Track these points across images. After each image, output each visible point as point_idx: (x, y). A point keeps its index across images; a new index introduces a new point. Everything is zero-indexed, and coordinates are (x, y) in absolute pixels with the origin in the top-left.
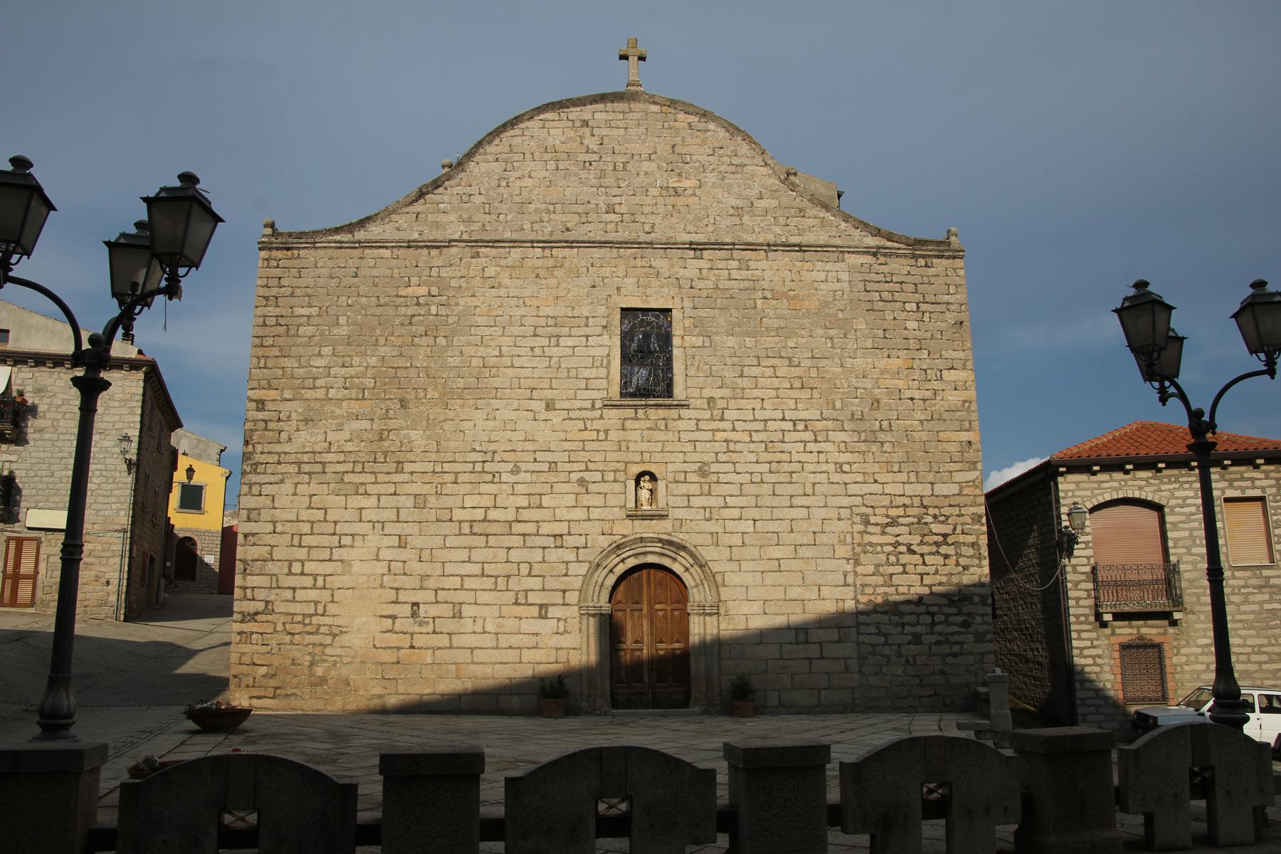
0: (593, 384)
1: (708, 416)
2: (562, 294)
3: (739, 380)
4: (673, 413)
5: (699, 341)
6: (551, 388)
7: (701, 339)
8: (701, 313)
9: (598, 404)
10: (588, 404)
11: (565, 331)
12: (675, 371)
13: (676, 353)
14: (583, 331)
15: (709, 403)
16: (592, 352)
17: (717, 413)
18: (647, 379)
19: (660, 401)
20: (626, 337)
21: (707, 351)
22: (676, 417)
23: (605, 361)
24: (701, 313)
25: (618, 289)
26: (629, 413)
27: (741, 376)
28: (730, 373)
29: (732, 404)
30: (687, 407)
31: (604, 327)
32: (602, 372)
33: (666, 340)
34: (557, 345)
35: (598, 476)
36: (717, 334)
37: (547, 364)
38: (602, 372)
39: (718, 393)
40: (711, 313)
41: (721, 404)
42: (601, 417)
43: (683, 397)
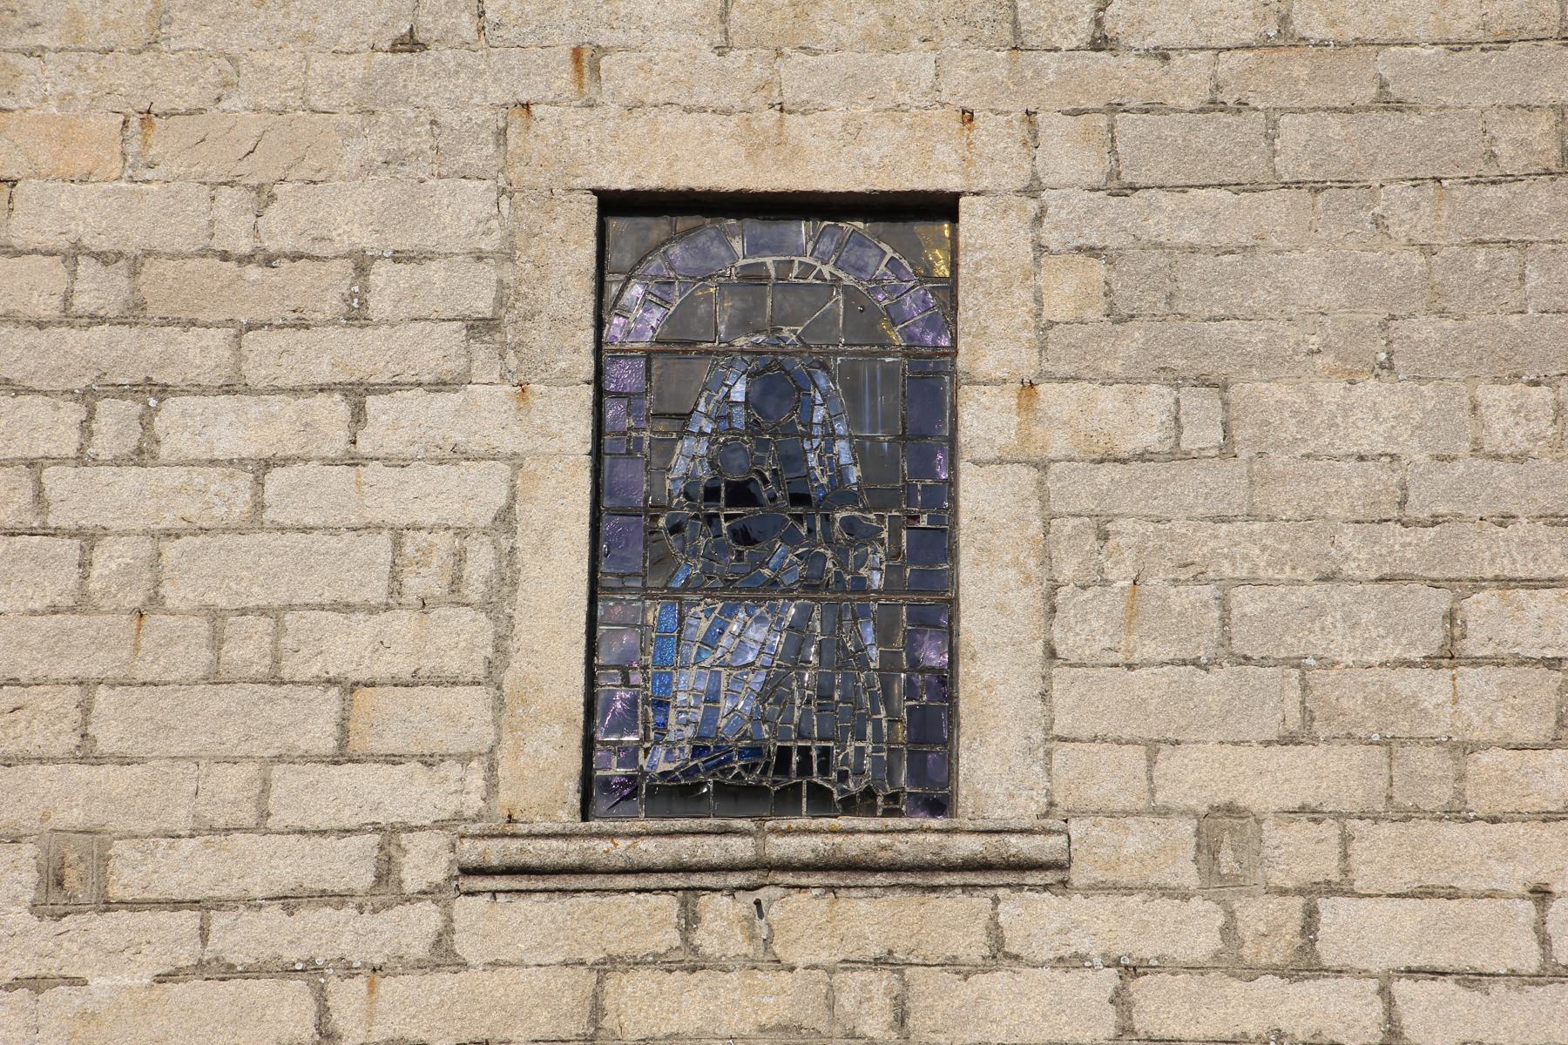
0: (393, 720)
1: (1203, 941)
2: (176, 91)
3: (1433, 689)
4: (953, 920)
5: (1141, 418)
6: (86, 754)
7: (1157, 399)
8: (1164, 219)
9: (423, 863)
10: (350, 865)
11: (203, 352)
12: (973, 623)
13: (984, 499)
14: (334, 353)
15: (1207, 848)
16: (387, 497)
17: (1267, 921)
18: (774, 690)
19: (862, 836)
20: (625, 411)
21: (1195, 487)
22: (972, 946)
23: (481, 562)
24: (1164, 219)
25: (585, 61)
26: (647, 920)
27: (1448, 657)
28: (1361, 637)
29: (1381, 853)
30: (1051, 872)
31: (480, 327)
32: (460, 637)
33: (922, 397)
34: (142, 456)
35: (393, 720)
36: (1272, 362)
37: (59, 584)
38: (460, 637)
39: (1270, 781)
40: (1235, 217)
41: (1300, 853)
42: (444, 954)
43: (1027, 809)
